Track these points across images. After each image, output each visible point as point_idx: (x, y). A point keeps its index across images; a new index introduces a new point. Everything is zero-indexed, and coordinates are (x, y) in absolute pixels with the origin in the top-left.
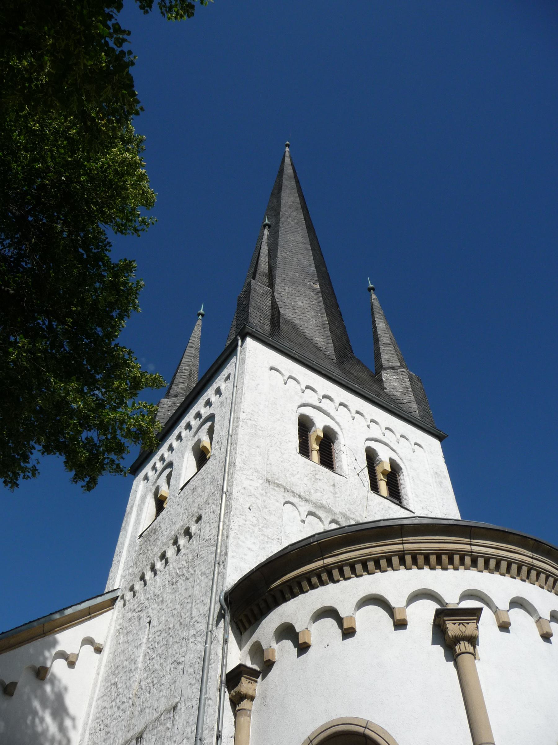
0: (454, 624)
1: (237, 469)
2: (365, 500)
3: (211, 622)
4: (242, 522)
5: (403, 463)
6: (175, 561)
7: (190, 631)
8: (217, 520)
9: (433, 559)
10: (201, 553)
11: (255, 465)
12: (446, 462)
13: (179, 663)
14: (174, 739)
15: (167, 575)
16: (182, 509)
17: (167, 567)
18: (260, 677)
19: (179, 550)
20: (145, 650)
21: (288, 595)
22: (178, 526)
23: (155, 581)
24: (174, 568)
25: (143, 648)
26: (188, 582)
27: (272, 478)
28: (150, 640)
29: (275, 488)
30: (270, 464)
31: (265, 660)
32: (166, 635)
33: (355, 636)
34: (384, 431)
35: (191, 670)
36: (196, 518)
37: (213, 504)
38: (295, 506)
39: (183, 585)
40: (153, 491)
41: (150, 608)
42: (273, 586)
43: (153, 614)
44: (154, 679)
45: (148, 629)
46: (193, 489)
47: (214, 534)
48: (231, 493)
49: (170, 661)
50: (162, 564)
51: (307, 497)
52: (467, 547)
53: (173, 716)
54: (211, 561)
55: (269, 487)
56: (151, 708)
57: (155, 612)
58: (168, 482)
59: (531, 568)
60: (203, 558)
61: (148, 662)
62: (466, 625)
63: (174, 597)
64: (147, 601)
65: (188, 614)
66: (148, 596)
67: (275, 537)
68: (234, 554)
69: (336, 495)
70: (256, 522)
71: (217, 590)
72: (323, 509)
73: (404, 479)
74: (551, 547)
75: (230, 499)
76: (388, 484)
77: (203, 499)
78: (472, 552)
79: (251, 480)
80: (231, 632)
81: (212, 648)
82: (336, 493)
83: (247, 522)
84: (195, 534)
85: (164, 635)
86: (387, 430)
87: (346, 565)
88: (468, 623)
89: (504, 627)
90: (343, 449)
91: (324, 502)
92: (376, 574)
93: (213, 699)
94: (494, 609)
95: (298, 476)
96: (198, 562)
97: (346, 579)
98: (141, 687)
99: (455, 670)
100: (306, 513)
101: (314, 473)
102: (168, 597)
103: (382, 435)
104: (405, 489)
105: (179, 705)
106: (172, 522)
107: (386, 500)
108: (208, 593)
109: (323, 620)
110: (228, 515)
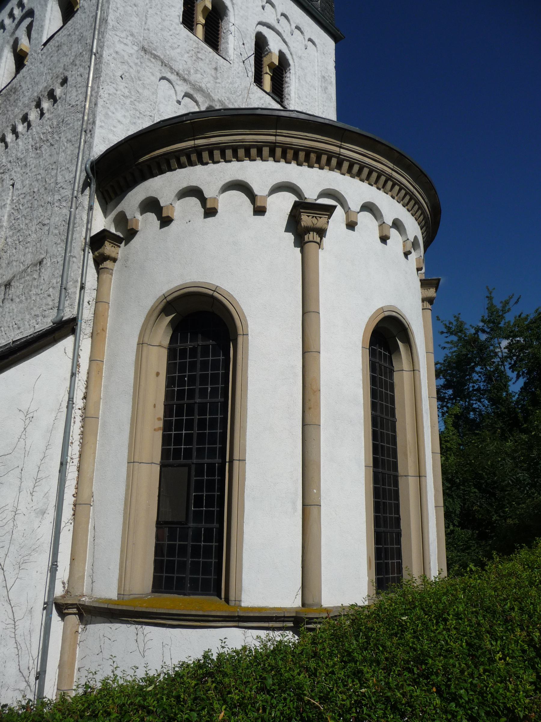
0: (308, 216)
1: (110, 27)
2: (246, 91)
3: (76, 189)
4: (112, 91)
5: (293, 58)
6: (39, 126)
7: (55, 196)
8: (85, 84)
9: (302, 155)
10: (66, 119)
11: (130, 26)
12: (336, 67)
13: (44, 225)
14: (41, 288)
15: (31, 139)
16: (46, 68)
17: (30, 131)
18: (123, 243)
19: (42, 114)
20: (9, 211)
21: (156, 171)
22: (41, 87)
23: (17, 144)
24: (38, 133)
25: (8, 209)
26: (53, 148)
27: (149, 46)
28: (15, 201)
29: (152, 59)
30: (148, 30)
31: (129, 228)
32: (30, 198)
33: (217, 216)
34: (279, 17)
35: (57, 231)
36: (61, 80)
37: (81, 65)
38: (172, 84)
39: (48, 151)
40: (12, 43)
41: (13, 171)
42: (141, 160)
43: (17, 178)
44: (20, 237)
45: (11, 191)
46: (58, 46)
47: (81, 100)
48: (101, 56)
49: (35, 222)
50: (24, 127)
51: (186, 77)
52: (337, 149)
53: (40, 269)
54: (77, 129)
55: (144, 57)
56: (18, 262)
57: (19, 175)
58: (29, 35)
59: (389, 178)
60: (69, 124)
61: (13, 222)
62: (318, 218)
63: (38, 162)
64: (9, 164)
65: (53, 180)
66: (10, 159)
67: (148, 113)
68: (103, 124)
69: (218, 81)
70: (128, 94)
71: (83, 159)
72: (202, 93)
73: (290, 77)
74: (412, 162)
75: (100, 62)
76: (272, 79)
77: (70, 59)
78: (340, 154)
79: (125, 44)
80: (96, 200)
81: (77, 213)
82: (217, 78)
83: (118, 92)
84: (60, 98)
85: (28, 198)
86: (283, 17)
87: (217, 148)
88: (320, 218)
89: (351, 226)
90: (232, 28)
91: (203, 86)
92: (245, 161)
93: (77, 257)
94: (346, 209)
95: (178, 50)
96: (63, 128)
97: (214, 162)
98: (7, 243)
99: (300, 255)
100: (183, 94)
101: (196, 50)
102: (31, 161)
103: (276, 21)
104: (289, 89)
105: (45, 260)
106: (34, 82)
107: (268, 96)
108: (73, 161)
109: (187, 199)
110: (98, 80)
